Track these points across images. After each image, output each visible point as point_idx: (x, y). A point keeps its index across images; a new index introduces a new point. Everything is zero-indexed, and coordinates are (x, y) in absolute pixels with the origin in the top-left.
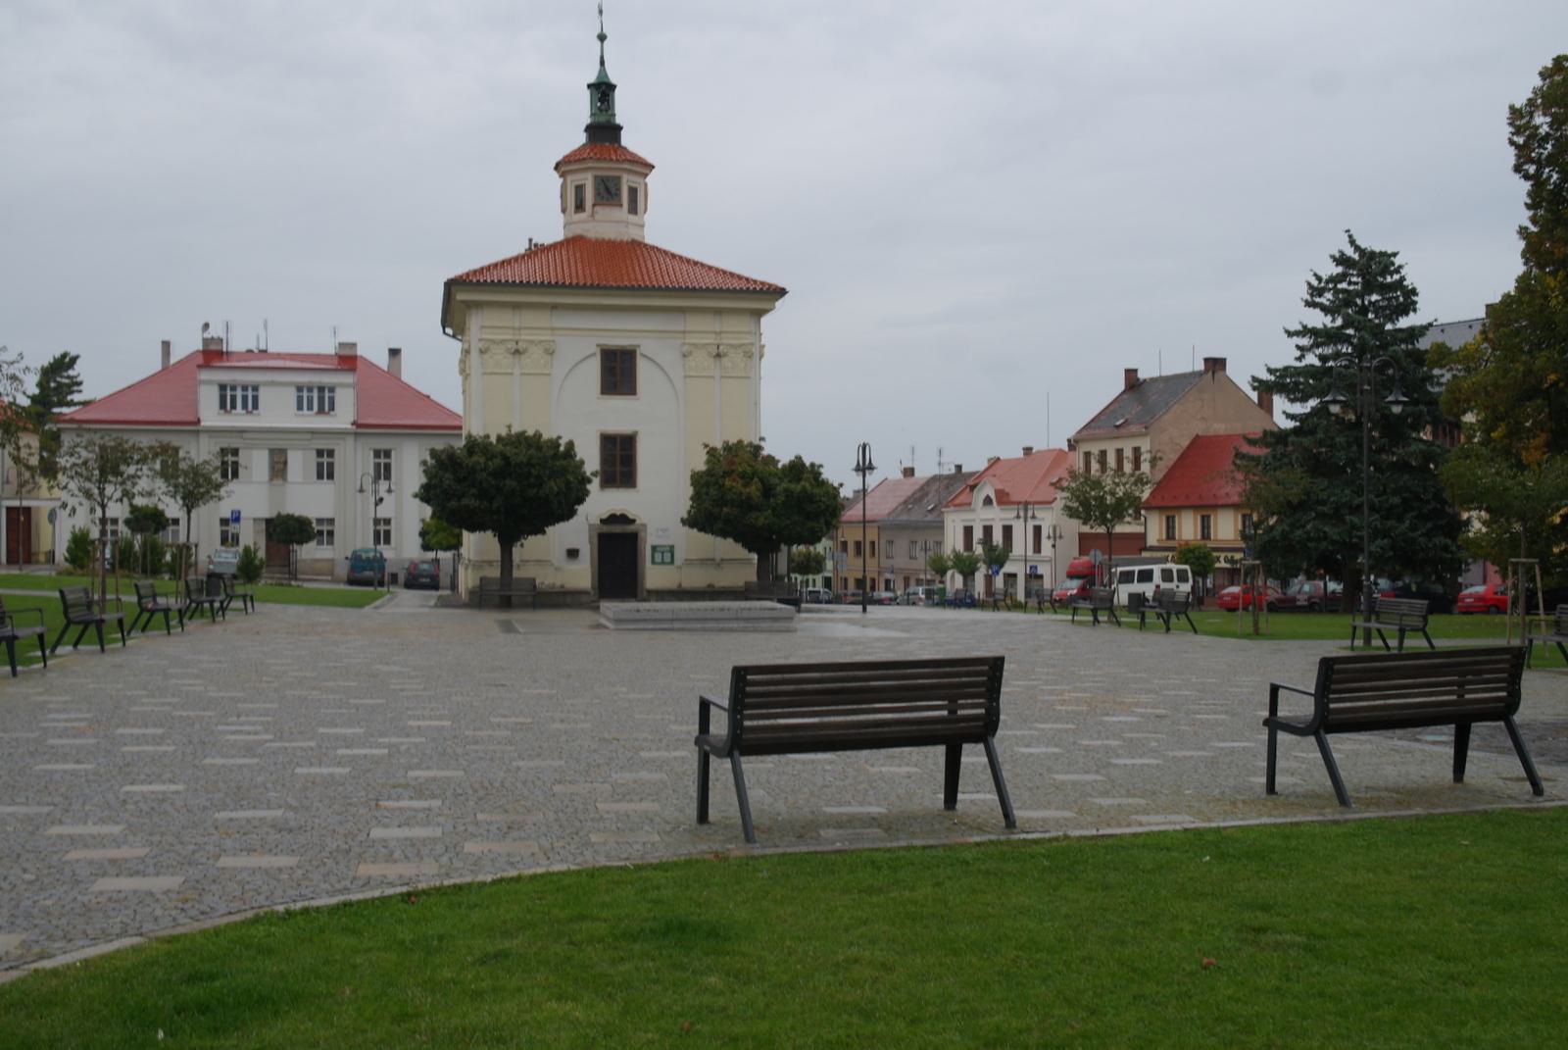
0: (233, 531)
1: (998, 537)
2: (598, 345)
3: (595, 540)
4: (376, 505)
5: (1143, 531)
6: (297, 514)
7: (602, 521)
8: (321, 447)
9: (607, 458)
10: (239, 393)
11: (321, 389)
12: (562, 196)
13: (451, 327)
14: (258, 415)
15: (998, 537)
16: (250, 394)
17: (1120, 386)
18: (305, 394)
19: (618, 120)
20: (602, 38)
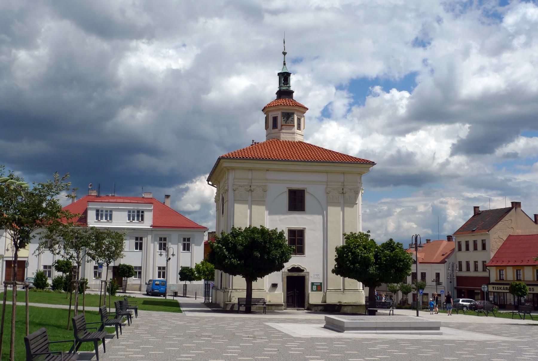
0: (99, 272)
2: (287, 188)
3: (285, 280)
4: (167, 261)
5: (416, 272)
6: (127, 264)
7: (288, 270)
8: (137, 236)
9: (292, 241)
10: (104, 213)
11: (138, 212)
16: (109, 213)
17: (472, 214)
18: (131, 214)
19: (292, 89)
20: (284, 54)
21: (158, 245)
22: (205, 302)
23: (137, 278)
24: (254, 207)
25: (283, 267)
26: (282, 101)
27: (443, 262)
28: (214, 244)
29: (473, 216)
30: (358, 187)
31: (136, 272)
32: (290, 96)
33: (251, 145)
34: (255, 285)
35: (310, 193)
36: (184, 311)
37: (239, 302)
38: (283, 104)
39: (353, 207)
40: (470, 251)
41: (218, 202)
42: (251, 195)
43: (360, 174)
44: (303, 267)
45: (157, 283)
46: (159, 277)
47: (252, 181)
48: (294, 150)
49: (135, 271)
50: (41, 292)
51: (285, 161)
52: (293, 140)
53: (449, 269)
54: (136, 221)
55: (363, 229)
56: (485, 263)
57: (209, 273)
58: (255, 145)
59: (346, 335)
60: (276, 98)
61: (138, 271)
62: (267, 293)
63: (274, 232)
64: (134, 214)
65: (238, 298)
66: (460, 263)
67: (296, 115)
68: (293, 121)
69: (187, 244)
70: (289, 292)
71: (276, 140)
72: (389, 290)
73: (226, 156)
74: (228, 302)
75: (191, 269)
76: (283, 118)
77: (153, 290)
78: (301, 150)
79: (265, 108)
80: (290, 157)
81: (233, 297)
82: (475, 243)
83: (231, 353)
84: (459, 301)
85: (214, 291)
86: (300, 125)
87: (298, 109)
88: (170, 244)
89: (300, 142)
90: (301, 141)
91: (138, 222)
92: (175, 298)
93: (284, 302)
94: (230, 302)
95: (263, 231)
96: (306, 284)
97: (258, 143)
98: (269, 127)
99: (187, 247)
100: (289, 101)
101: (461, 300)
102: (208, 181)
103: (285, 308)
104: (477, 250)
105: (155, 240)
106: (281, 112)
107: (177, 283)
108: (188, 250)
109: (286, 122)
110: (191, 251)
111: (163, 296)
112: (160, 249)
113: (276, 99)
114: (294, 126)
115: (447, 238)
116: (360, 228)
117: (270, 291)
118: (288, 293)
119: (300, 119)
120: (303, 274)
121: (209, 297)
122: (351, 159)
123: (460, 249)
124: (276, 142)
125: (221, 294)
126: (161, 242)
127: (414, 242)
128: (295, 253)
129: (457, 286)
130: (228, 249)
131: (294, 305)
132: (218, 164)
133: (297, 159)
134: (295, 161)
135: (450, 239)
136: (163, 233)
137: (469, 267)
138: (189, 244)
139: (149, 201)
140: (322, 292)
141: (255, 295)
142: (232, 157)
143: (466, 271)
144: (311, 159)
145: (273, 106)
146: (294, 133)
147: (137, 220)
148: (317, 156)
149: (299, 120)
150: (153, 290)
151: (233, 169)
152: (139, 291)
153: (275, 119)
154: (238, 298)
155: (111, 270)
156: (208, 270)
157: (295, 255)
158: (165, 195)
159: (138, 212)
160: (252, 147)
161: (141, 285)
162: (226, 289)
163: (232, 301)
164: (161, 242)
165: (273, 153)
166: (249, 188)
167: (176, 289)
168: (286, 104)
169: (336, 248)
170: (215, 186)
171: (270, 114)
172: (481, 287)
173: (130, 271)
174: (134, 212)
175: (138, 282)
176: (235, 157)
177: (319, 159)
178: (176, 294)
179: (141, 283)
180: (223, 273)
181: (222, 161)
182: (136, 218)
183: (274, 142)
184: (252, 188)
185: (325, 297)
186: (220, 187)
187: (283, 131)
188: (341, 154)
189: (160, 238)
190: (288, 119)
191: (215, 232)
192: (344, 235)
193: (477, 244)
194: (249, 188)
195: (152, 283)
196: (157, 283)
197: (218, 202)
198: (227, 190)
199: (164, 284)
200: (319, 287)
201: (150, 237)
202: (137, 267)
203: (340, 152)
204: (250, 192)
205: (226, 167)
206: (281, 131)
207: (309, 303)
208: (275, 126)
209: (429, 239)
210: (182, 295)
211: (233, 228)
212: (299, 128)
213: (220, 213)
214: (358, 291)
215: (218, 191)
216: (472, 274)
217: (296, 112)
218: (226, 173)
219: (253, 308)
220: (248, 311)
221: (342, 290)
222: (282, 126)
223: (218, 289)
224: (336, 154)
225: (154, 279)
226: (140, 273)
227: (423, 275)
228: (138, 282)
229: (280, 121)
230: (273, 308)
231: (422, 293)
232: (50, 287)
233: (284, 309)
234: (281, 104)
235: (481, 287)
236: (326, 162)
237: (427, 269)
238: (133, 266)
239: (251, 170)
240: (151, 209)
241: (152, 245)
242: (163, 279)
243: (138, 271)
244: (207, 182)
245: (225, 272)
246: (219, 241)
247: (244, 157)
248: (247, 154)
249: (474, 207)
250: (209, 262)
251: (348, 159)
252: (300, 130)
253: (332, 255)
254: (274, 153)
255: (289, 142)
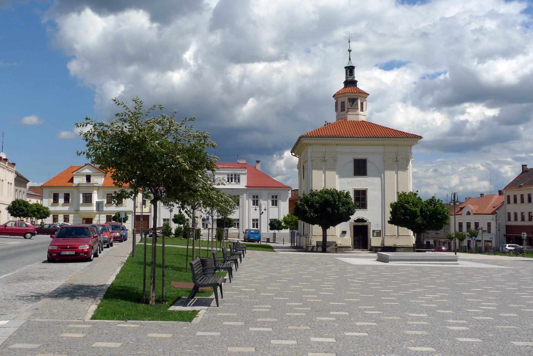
1: (473, 227)
2: (353, 158)
3: (352, 228)
7: (355, 221)
9: (357, 199)
11: (235, 175)
12: (336, 106)
13: (294, 153)
14: (240, 184)
15: (473, 227)
19: (356, 79)
20: (350, 51)
21: (252, 201)
22: (291, 246)
23: (236, 228)
24: (327, 172)
25: (350, 218)
26: (349, 89)
27: (494, 213)
28: (298, 202)
29: (521, 174)
30: (409, 156)
31: (235, 223)
32: (355, 85)
33: (325, 125)
34: (328, 231)
35: (371, 162)
36: (277, 251)
37: (317, 245)
38: (349, 92)
39: (405, 171)
40: (518, 204)
41: (300, 169)
42: (325, 164)
43: (411, 146)
44: (366, 218)
45: (253, 232)
46: (253, 227)
47: (326, 154)
48: (358, 128)
49: (235, 222)
50: (167, 238)
51: (351, 137)
52: (358, 120)
53: (500, 219)
54: (233, 182)
55: (413, 190)
56: (530, 214)
57: (294, 223)
58: (327, 124)
59: (390, 264)
60: (343, 87)
61: (236, 222)
62: (339, 238)
63: (341, 193)
64: (232, 177)
65: (317, 242)
66: (509, 214)
67: (359, 100)
68: (357, 105)
69: (275, 200)
70: (355, 237)
71: (344, 121)
72: (446, 238)
73: (305, 135)
74: (309, 245)
75: (279, 221)
76: (349, 103)
77: (249, 237)
78: (364, 128)
79: (335, 95)
80: (354, 134)
81: (313, 241)
82: (522, 196)
83: (311, 270)
84: (506, 246)
85: (298, 237)
86: (363, 107)
87: (361, 95)
88: (261, 200)
89: (363, 121)
90: (364, 120)
91: (235, 183)
92: (268, 244)
93: (352, 245)
94: (311, 244)
95: (333, 193)
96: (368, 231)
97: (330, 123)
98: (338, 110)
99: (275, 203)
100: (353, 89)
101: (507, 245)
102: (292, 152)
103: (352, 249)
104: (524, 203)
105: (249, 198)
106: (348, 98)
107: (268, 232)
108: (276, 205)
109: (352, 106)
110: (279, 206)
111: (257, 242)
112: (254, 205)
113: (344, 88)
114: (358, 109)
115: (498, 192)
116: (410, 189)
117: (341, 236)
118: (355, 238)
119: (363, 103)
120: (366, 224)
121: (294, 243)
122: (403, 134)
123: (509, 202)
124: (344, 122)
125: (303, 239)
126: (254, 199)
127: (453, 199)
128: (360, 207)
129: (506, 234)
130: (309, 207)
131: (360, 247)
132: (298, 143)
133: (360, 135)
134: (358, 137)
135: (501, 193)
136: (256, 192)
137: (517, 218)
138: (277, 200)
139: (243, 167)
140: (381, 237)
141: (329, 239)
142: (310, 136)
143: (521, 221)
144: (371, 135)
145: (341, 93)
146: (358, 114)
147: (235, 182)
148: (376, 133)
149: (362, 104)
150: (249, 237)
151: (311, 144)
152: (238, 238)
153: (343, 103)
154: (317, 242)
155: (215, 222)
156: (293, 221)
157: (359, 210)
158: (256, 161)
159: (235, 175)
160: (325, 127)
161: (239, 233)
162: (307, 235)
163: (312, 244)
164: (254, 199)
165: (341, 131)
166: (323, 159)
167: (267, 236)
168: (351, 92)
169: (391, 204)
170: (298, 156)
171: (339, 100)
172: (521, 234)
173: (230, 223)
174: (232, 175)
175: (237, 231)
176: (312, 136)
177: (377, 135)
178: (268, 241)
179: (239, 232)
180: (305, 223)
181: (302, 139)
182: (233, 180)
183: (342, 122)
184: (326, 158)
185: (383, 241)
186: (301, 158)
187: (349, 113)
188: (395, 130)
189: (253, 196)
190: (353, 104)
191: (298, 190)
192: (398, 193)
193: (523, 198)
194: (323, 159)
195: (248, 232)
196: (252, 231)
197: (300, 169)
198: (307, 161)
199: (258, 233)
200: (379, 234)
201: (245, 195)
202: (235, 219)
203: (394, 129)
204: (324, 162)
205: (305, 143)
206: (348, 113)
207: (371, 246)
208: (343, 110)
209: (482, 193)
210: (272, 242)
211: (311, 190)
212: (362, 110)
213: (302, 178)
214: (409, 236)
215: (300, 160)
216: (519, 223)
217: (359, 98)
218: (305, 148)
219: (328, 249)
220: (324, 251)
221: (397, 236)
222: (348, 109)
223: (302, 236)
224: (391, 131)
225: (249, 229)
226: (238, 224)
227: (477, 225)
228: (237, 231)
229: (347, 104)
230: (343, 249)
231: (474, 239)
232: (173, 236)
233: (352, 250)
234: (347, 92)
235: (521, 234)
236: (383, 137)
237: (479, 220)
238: (232, 218)
239: (324, 145)
240: (245, 172)
241: (247, 201)
242: (256, 229)
243: (236, 222)
244: (291, 153)
245: (306, 223)
246: (302, 200)
247: (319, 136)
248: (321, 133)
249: (522, 165)
250: (294, 215)
251: (401, 134)
252: (363, 112)
253: (389, 209)
254: (342, 131)
255: (354, 121)
